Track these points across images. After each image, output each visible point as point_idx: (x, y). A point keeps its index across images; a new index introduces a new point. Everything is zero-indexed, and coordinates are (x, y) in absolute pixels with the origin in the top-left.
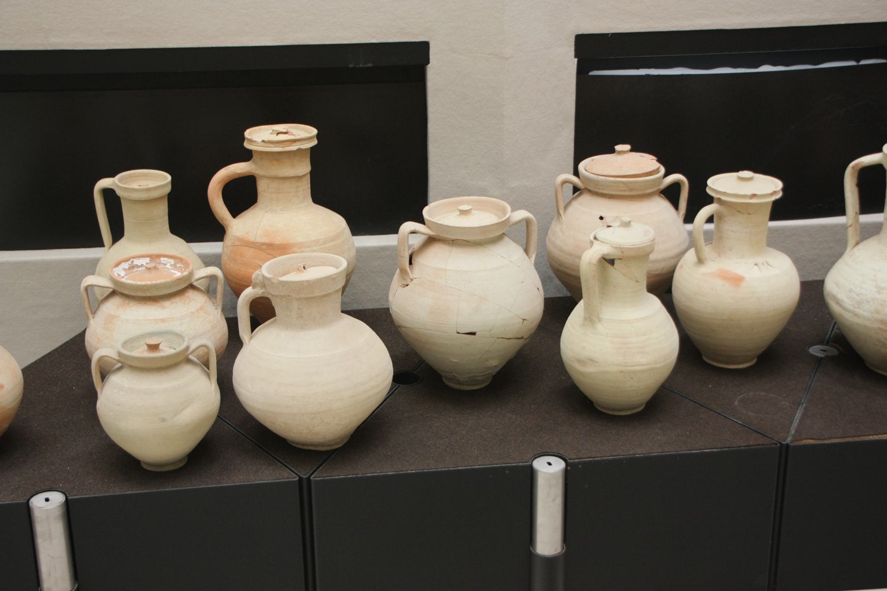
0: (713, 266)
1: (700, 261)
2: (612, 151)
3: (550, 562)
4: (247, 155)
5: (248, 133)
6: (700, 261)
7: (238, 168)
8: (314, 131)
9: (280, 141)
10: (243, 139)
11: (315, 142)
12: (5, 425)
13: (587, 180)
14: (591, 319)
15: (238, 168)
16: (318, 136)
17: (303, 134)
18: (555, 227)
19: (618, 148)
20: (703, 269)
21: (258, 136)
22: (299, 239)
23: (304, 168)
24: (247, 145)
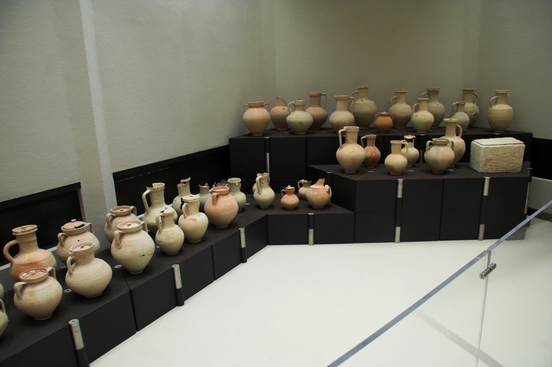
0: (188, 218)
1: (185, 217)
2: (70, 221)
3: (81, 350)
4: (14, 238)
5: (13, 230)
6: (185, 217)
7: (12, 242)
8: (36, 226)
9: (26, 230)
10: (12, 232)
11: (36, 230)
12: (3, 331)
13: (67, 232)
14: (160, 232)
15: (12, 242)
16: (37, 227)
17: (32, 228)
18: (425, 155)
19: (72, 220)
20: (186, 219)
21: (18, 230)
22: (40, 259)
23: (35, 238)
24: (13, 234)
